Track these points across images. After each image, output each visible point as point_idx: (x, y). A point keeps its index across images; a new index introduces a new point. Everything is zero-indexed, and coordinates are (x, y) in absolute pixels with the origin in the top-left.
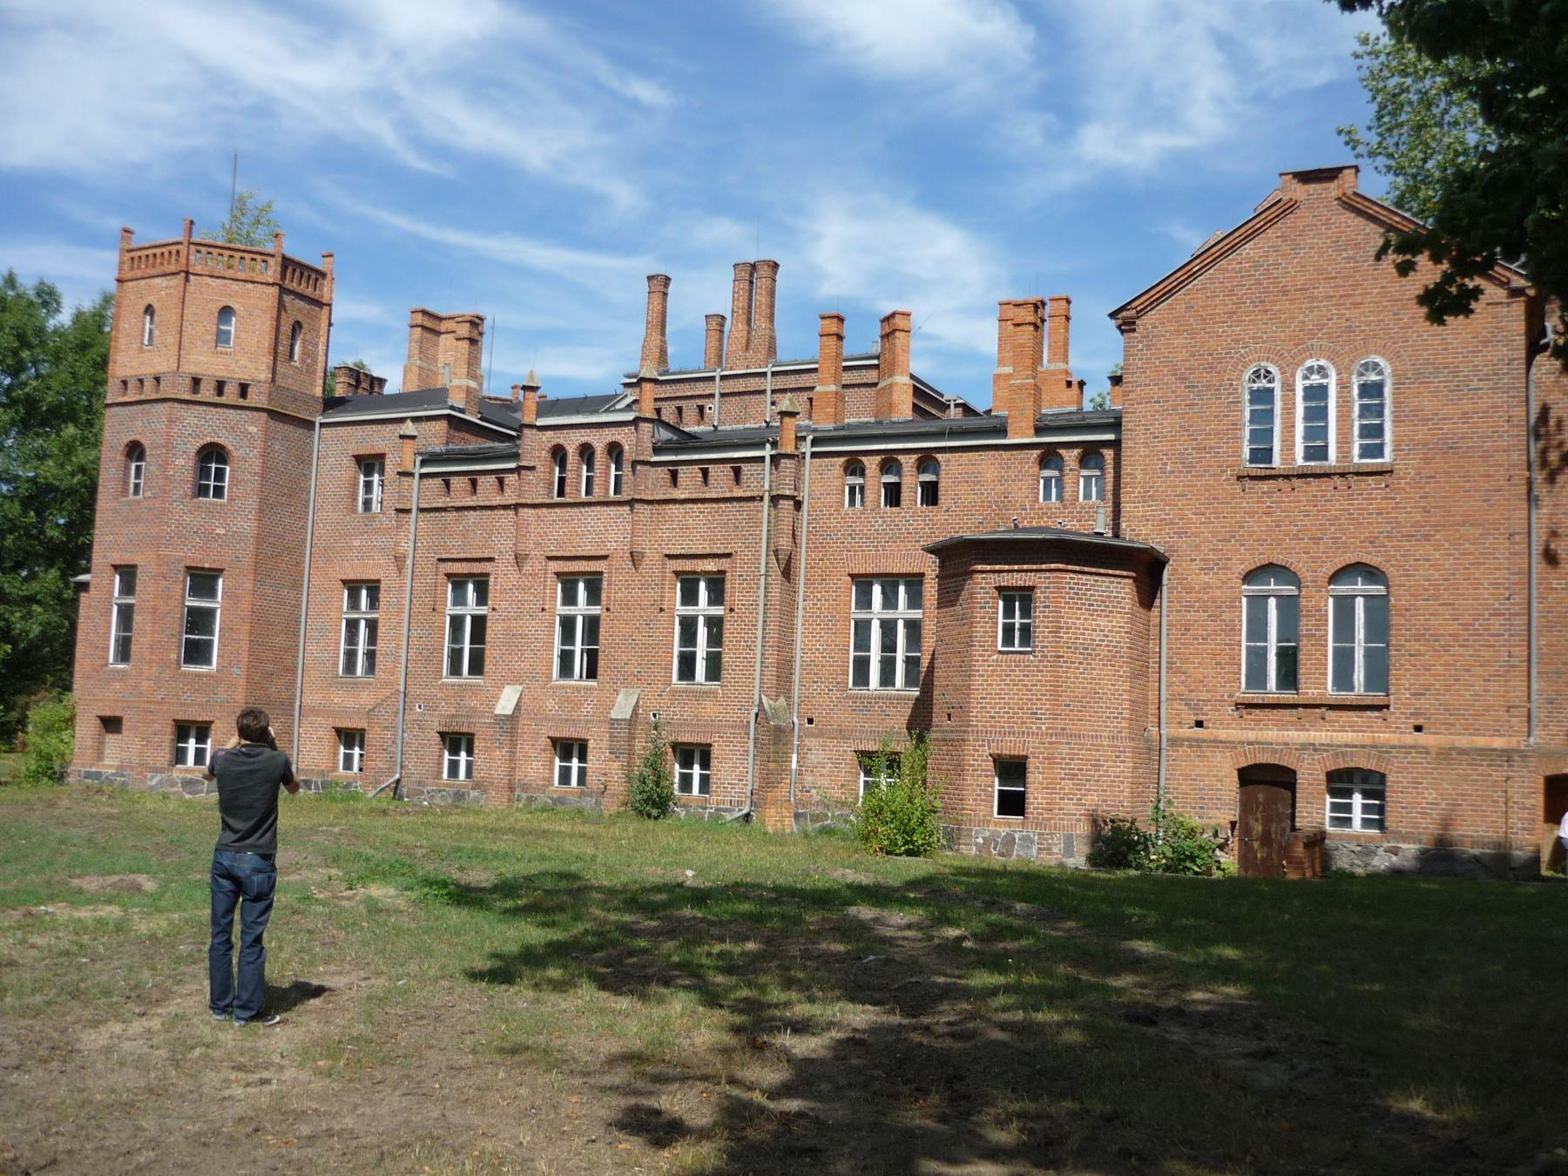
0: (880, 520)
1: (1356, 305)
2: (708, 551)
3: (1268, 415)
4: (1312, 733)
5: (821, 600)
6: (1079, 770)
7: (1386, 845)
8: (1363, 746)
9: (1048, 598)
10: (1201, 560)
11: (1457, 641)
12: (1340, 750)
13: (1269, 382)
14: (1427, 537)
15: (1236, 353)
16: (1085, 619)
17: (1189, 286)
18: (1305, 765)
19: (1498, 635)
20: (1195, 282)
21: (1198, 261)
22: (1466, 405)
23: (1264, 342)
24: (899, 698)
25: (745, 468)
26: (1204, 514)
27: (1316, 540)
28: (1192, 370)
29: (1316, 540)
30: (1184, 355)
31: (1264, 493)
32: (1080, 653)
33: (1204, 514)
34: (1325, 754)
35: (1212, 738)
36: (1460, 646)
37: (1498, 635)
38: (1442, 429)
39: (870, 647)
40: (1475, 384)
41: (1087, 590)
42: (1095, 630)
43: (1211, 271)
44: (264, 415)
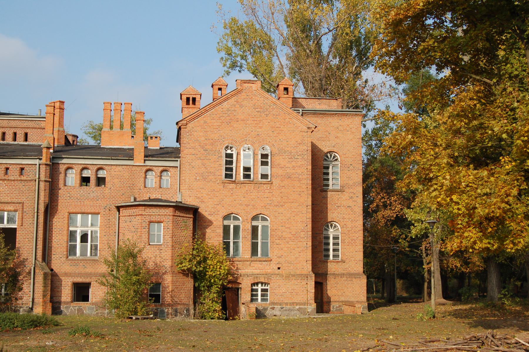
0: (82, 191)
1: (261, 127)
2: (10, 201)
3: (231, 163)
4: (246, 271)
5: (56, 222)
6: (179, 285)
7: (270, 307)
8: (263, 275)
9: (169, 225)
10: (209, 211)
11: (291, 240)
12: (255, 276)
13: (232, 151)
14: (282, 206)
15: (221, 140)
16: (180, 233)
17: (205, 115)
18: (244, 281)
19: (303, 238)
20: (207, 113)
21: (209, 106)
22: (294, 164)
23: (230, 137)
24: (78, 260)
25: (26, 168)
26: (210, 195)
27: (247, 205)
28: (206, 144)
29: (247, 205)
30: (203, 139)
31: (230, 189)
32: (179, 245)
33: (210, 195)
34: (251, 277)
35: (265, 273)
36: (292, 241)
37: (303, 238)
38: (286, 171)
39: (76, 240)
40: (296, 157)
41: (181, 222)
42: (182, 237)
43: (213, 110)
44: (170, 211)
